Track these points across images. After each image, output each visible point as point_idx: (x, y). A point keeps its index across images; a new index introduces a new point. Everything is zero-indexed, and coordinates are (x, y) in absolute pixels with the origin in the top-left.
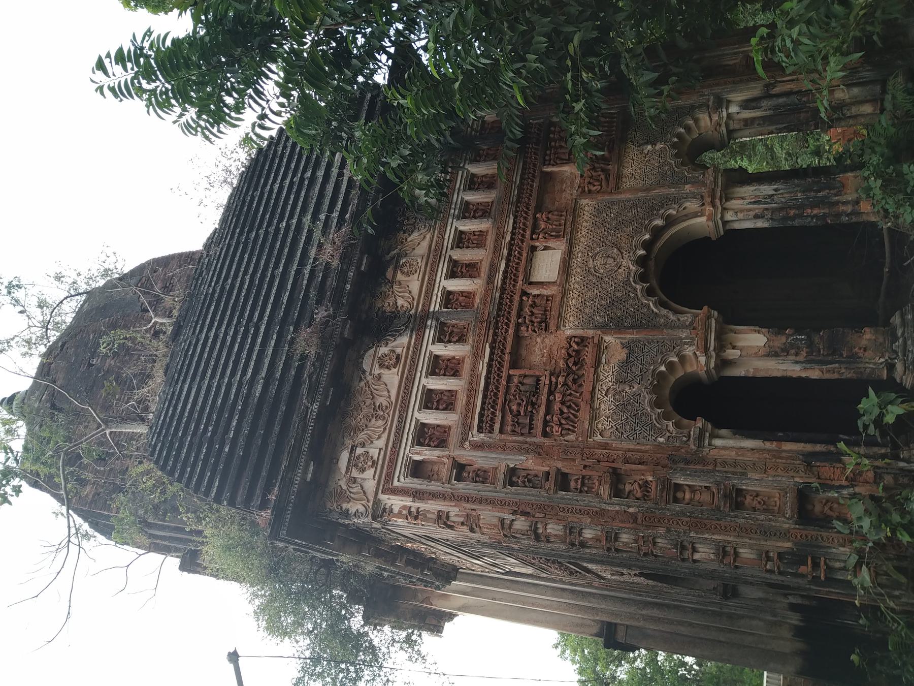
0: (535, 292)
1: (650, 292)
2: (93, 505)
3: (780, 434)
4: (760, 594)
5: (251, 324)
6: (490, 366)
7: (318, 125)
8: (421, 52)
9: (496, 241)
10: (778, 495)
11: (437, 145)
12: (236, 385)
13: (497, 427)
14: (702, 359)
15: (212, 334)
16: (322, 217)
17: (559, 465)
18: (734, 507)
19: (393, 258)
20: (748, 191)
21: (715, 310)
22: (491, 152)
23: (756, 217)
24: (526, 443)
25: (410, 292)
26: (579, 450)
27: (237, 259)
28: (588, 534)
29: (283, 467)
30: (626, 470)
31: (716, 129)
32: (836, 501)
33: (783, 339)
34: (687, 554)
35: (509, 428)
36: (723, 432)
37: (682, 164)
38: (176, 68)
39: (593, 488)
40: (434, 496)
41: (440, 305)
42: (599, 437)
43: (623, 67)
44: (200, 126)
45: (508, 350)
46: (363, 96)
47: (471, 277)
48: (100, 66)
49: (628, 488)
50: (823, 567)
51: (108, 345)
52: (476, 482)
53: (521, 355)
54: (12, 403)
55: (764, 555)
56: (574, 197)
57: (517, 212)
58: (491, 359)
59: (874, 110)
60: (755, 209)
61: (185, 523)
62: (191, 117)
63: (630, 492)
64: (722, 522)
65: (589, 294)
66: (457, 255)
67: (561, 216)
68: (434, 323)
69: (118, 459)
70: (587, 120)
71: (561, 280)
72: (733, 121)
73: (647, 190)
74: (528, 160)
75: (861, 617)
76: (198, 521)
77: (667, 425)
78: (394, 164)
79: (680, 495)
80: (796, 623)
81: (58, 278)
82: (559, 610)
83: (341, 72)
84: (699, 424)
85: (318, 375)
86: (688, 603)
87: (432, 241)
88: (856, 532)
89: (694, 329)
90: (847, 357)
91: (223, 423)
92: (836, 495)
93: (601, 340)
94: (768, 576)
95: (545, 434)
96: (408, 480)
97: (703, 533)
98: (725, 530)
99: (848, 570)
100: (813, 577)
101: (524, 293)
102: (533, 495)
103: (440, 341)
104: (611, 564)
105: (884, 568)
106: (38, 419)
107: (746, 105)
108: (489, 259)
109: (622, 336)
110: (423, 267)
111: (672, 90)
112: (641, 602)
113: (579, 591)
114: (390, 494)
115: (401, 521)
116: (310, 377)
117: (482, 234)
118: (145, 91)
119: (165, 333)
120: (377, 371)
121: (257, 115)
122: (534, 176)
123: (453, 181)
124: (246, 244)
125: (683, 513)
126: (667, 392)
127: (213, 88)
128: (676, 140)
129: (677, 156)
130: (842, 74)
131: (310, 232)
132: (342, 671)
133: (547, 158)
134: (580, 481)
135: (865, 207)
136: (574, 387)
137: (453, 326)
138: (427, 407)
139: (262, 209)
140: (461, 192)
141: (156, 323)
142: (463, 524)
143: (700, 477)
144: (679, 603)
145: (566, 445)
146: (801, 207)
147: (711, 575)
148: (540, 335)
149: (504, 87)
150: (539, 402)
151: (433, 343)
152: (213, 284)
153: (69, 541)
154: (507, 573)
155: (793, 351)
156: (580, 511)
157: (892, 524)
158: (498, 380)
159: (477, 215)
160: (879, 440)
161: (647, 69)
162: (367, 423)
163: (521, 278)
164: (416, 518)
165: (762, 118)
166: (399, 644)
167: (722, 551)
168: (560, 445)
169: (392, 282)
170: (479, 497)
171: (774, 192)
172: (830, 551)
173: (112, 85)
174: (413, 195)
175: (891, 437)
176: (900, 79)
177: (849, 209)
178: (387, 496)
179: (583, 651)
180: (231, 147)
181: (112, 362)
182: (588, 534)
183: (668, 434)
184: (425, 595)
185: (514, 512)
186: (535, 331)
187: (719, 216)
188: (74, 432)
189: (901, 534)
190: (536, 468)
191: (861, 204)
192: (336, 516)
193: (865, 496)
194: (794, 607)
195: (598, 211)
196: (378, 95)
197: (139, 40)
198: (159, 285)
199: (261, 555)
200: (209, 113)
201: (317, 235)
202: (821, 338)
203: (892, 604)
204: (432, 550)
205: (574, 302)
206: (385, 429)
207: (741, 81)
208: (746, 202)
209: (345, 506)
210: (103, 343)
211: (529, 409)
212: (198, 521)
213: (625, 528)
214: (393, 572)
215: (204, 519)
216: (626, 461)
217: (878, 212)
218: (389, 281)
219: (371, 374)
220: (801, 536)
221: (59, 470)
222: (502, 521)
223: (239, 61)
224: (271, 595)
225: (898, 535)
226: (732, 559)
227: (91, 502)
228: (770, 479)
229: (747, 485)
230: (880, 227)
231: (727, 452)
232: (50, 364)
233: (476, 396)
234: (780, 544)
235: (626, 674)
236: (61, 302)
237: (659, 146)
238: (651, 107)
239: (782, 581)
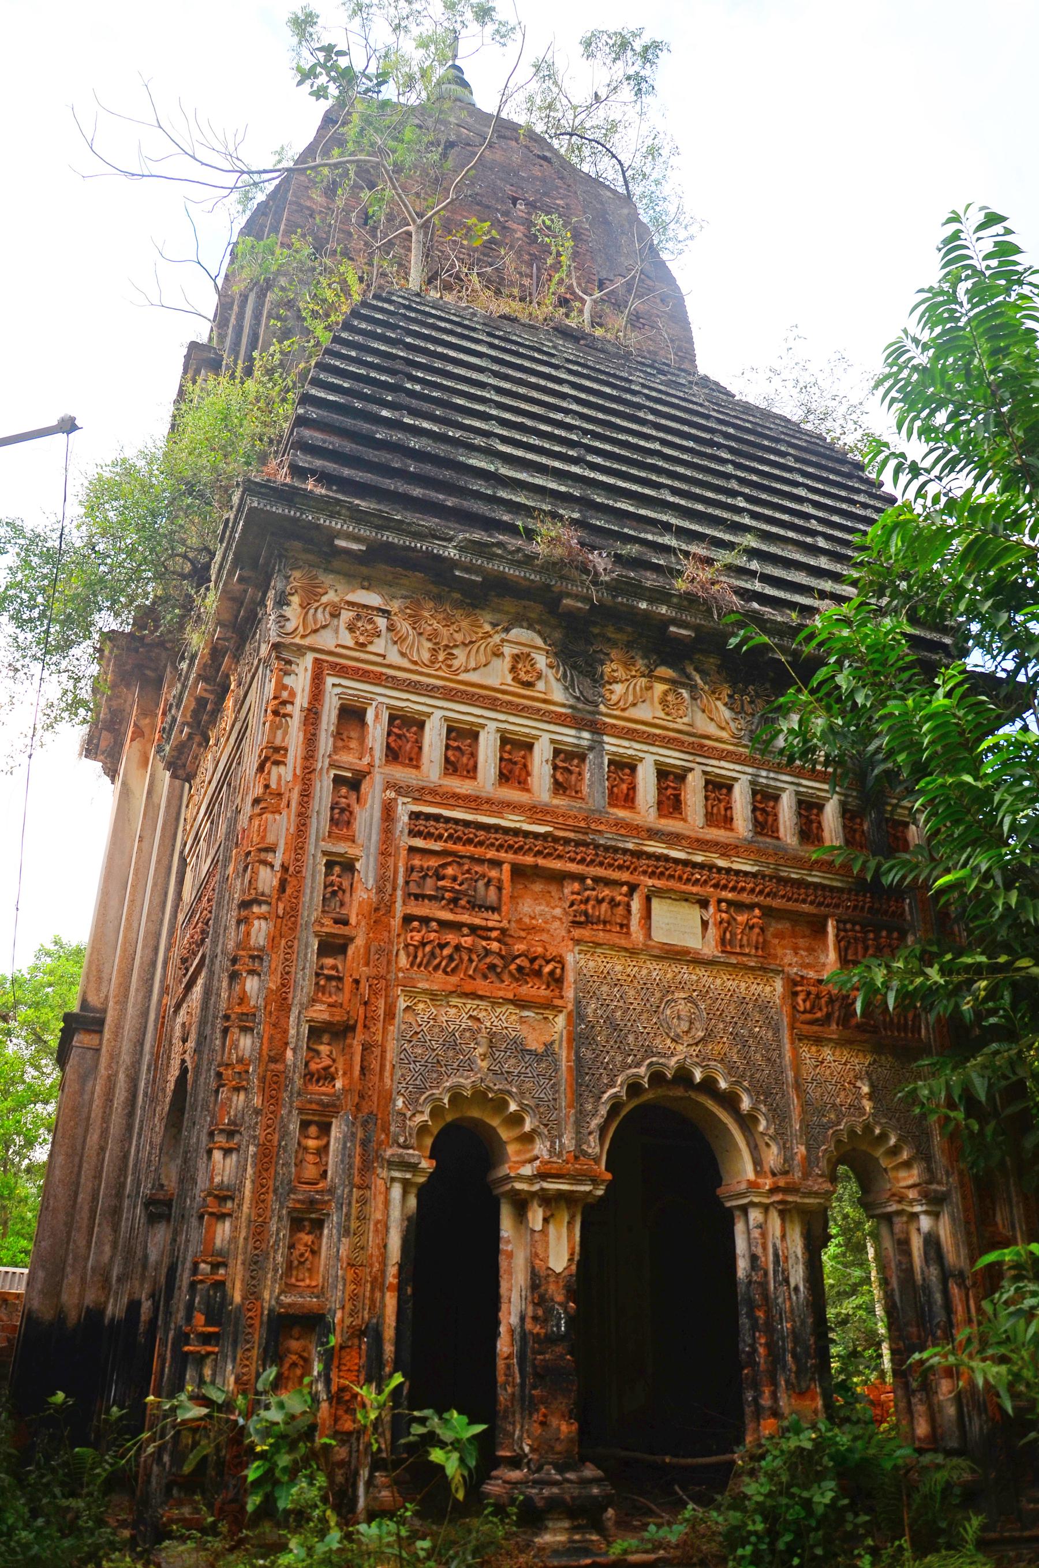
0: (636, 905)
1: (634, 1088)
2: (294, 207)
3: (409, 1291)
4: (153, 1257)
5: (582, 452)
6: (516, 832)
7: (904, 558)
8: (1019, 724)
9: (717, 844)
10: (314, 1284)
11: (872, 748)
12: (486, 427)
13: (419, 843)
14: (527, 1170)
15: (566, 389)
16: (754, 565)
17: (360, 942)
18: (295, 1215)
19: (689, 677)
20: (796, 1245)
21: (606, 1190)
22: (857, 836)
23: (754, 1258)
24: (394, 889)
25: (634, 705)
26: (383, 972)
27: (686, 429)
28: (251, 984)
29: (357, 502)
30: (351, 1046)
31: (893, 1195)
32: (307, 1370)
33: (559, 1298)
34: (220, 1139)
35: (417, 862)
36: (412, 1202)
37: (839, 1142)
38: (993, 333)
39: (323, 994)
40: (311, 741)
41: (614, 754)
42: (403, 1005)
43: (994, 1046)
44: (900, 370)
45: (541, 861)
46: (945, 630)
47: (660, 803)
48: (992, 219)
49: (324, 1049)
50: (204, 1349)
51: (548, 228)
52: (332, 809)
53: (533, 882)
54: (457, 83)
55: (220, 1259)
56: (786, 969)
57: (764, 877)
58: (527, 834)
59: (919, 1439)
60: (766, 1255)
61: (265, 349)
62: (913, 358)
63: (318, 1052)
64: (271, 1196)
65: (632, 993)
66: (695, 782)
67: (757, 948)
68: (585, 743)
69: (366, 244)
70: (911, 988)
71: (654, 947)
72: (907, 1222)
73: (797, 1086)
74: (845, 896)
75: (121, 1408)
76: (267, 370)
77: (422, 1112)
78: (841, 680)
79: (313, 1130)
80: (109, 1311)
81: (653, 152)
82: (124, 943)
83: (986, 596)
84: (424, 1164)
85: (502, 557)
86: (138, 1146)
87: (717, 740)
88: (259, 1402)
89: (576, 1158)
90: (532, 1396)
91: (425, 406)
92: (315, 1373)
93: (557, 1009)
94: (188, 1265)
95: (408, 919)
96: (335, 699)
97: (255, 1165)
98: (258, 1200)
99: (199, 1387)
100: (187, 1335)
101: (633, 888)
102: (311, 898)
103: (557, 752)
104: (203, 1022)
105: (204, 1442)
106: (430, 122)
107: (932, 1242)
108: (687, 833)
109: (564, 1044)
110: (675, 726)
111: (958, 1125)
112: (138, 1072)
113: (153, 974)
114: (313, 671)
115: (270, 688)
116: (500, 544)
117: (727, 821)
118: (954, 286)
119: (567, 316)
120: (508, 650)
121: (918, 461)
122: (820, 904)
123: (814, 775)
124: (711, 443)
125: (285, 1134)
126: (475, 1113)
127: (960, 392)
128: (877, 1131)
129: (852, 1132)
130: (980, 1382)
131: (730, 546)
132: (32, 598)
133: (849, 926)
134: (333, 973)
135: (768, 1426)
136: (482, 966)
137: (580, 774)
138: (450, 730)
139: (766, 469)
140: (795, 788)
141: (583, 302)
142: (267, 786)
143: (342, 1161)
144: (136, 1130)
145: (391, 951)
146: (769, 1328)
147: (187, 1178)
148: (566, 913)
149: (964, 856)
150: (459, 910)
151: (552, 741)
152: (646, 391)
153: (243, 172)
154: (183, 862)
155: (540, 1312)
156: (288, 973)
157: (273, 1455)
158: (493, 845)
159: (758, 813)
160: (403, 1441)
161: (990, 1086)
162: (426, 636)
163: (659, 883)
164: (276, 713)
165: (910, 1270)
166: (71, 688)
167: (224, 1195)
168: (391, 942)
169: (650, 675)
170: (309, 812)
171: (792, 1285)
172: (229, 1361)
173: (962, 235)
174: (789, 710)
175: (407, 1459)
176: (967, 1476)
177: (766, 1401)
178: (310, 667)
179: (51, 985)
180: (866, 421)
181: (519, 235)
182: (251, 984)
183: (409, 1114)
184: (147, 731)
185: (285, 868)
186: (572, 904)
187: (756, 1200)
188: (410, 177)
189: (258, 1467)
190: (355, 905)
191: (772, 1420)
192: (280, 586)
193: (315, 1416)
194: (134, 1306)
195: (763, 1007)
196: (949, 655)
197: (1031, 279)
198: (643, 308)
199: (214, 469)
200: (922, 384)
201: (726, 557)
202: (561, 1357)
203: (150, 1450)
204: (223, 740)
205: (618, 968)
206: (415, 663)
207: (968, 1234)
208: (778, 1242)
209: (295, 600)
210: (552, 221)
211: (447, 895)
212: (267, 370)
213: (262, 1044)
214: (187, 678)
215: (270, 380)
216: (366, 1048)
217: (760, 1446)
218: (652, 671)
219: (503, 641)
220: (251, 1318)
221: (350, 155)
222: (271, 849)
223: (1004, 434)
224: (152, 486)
225: (256, 1464)
226: (215, 1210)
227: (299, 205)
228: (340, 1272)
229: (330, 1236)
230: (735, 1449)
231: (381, 1206)
232: (517, 140)
233: (468, 809)
234: (238, 1285)
235: (15, 1053)
236: (614, 156)
237: (868, 1105)
238: (931, 1092)
239: (180, 1288)
